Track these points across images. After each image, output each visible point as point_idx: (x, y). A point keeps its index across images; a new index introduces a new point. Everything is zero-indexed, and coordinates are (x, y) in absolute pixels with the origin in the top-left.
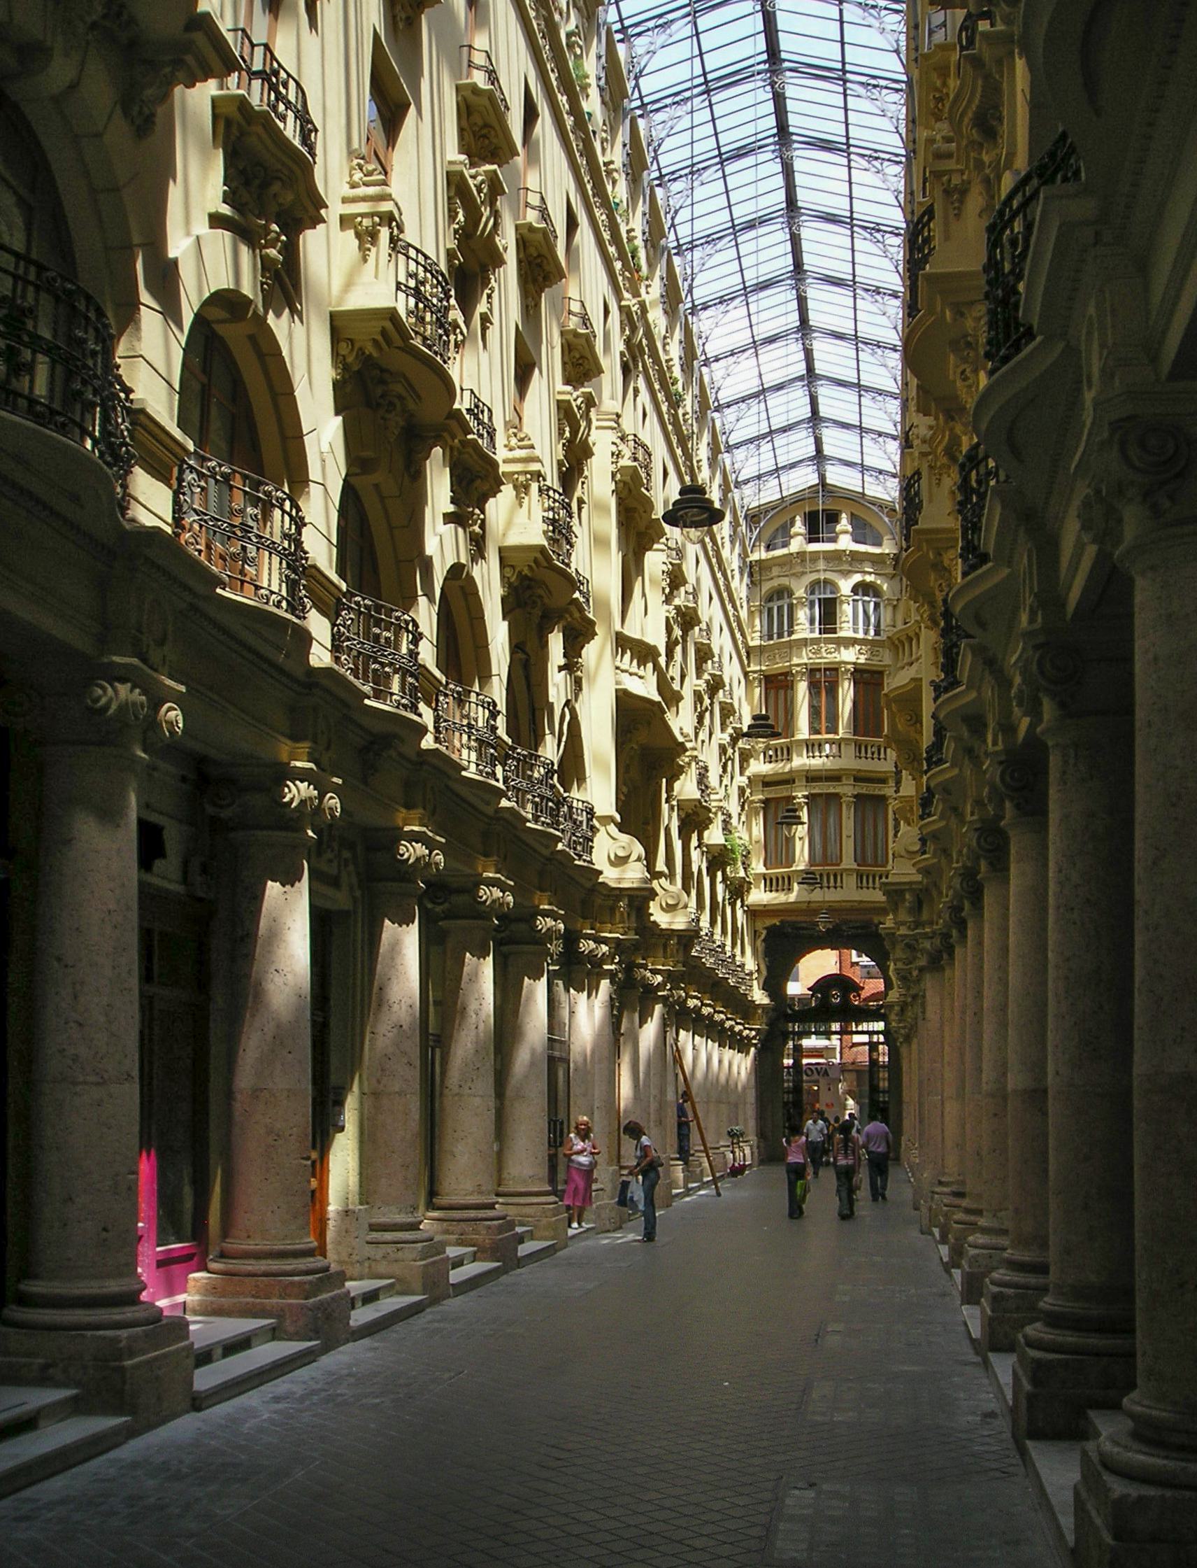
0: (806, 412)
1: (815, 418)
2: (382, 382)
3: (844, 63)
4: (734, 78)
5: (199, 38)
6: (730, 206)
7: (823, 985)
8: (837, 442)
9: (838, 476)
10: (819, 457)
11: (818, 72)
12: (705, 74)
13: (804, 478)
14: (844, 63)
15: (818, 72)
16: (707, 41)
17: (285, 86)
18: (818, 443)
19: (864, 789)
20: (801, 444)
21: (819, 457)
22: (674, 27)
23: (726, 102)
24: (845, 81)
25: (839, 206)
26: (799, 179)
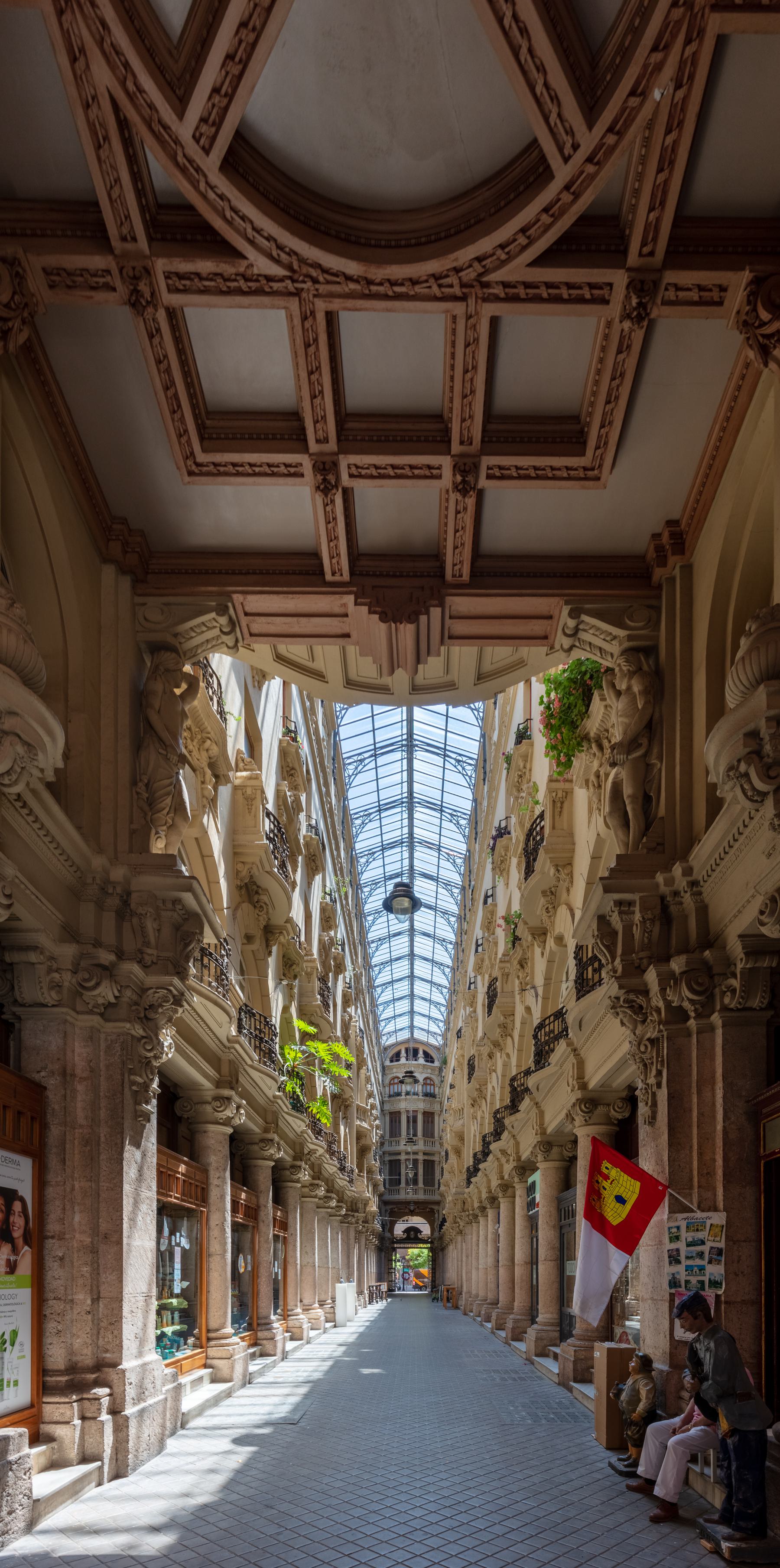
0: (406, 951)
1: (412, 996)
2: (257, 893)
3: (445, 744)
4: (392, 845)
5: (288, 925)
6: (373, 716)
7: (408, 1231)
8: (419, 1021)
9: (418, 1035)
10: (412, 1027)
11: (428, 845)
12: (375, 744)
13: (404, 1035)
14: (445, 744)
15: (428, 845)
16: (384, 822)
17: (211, 677)
18: (412, 968)
19: (426, 1158)
20: (404, 1022)
21: (412, 1027)
22: (366, 761)
23: (395, 942)
24: (445, 756)
25: (430, 930)
26: (416, 776)
